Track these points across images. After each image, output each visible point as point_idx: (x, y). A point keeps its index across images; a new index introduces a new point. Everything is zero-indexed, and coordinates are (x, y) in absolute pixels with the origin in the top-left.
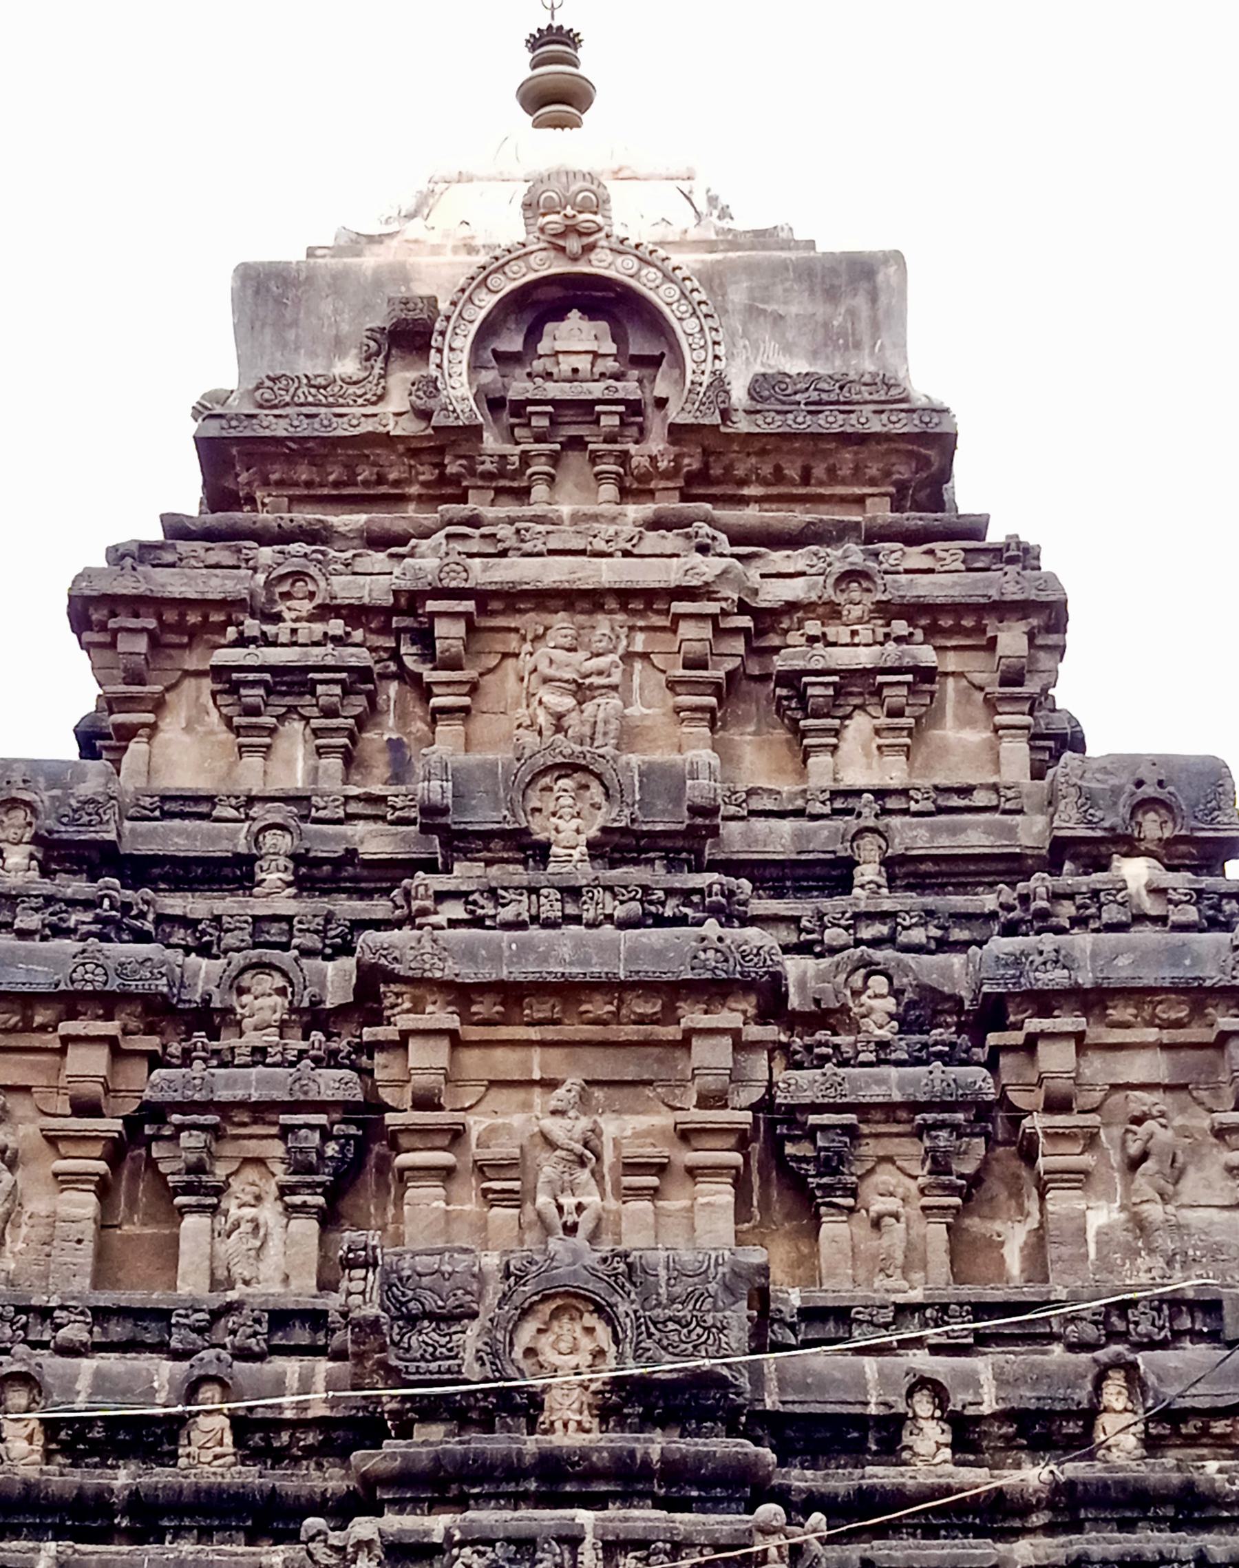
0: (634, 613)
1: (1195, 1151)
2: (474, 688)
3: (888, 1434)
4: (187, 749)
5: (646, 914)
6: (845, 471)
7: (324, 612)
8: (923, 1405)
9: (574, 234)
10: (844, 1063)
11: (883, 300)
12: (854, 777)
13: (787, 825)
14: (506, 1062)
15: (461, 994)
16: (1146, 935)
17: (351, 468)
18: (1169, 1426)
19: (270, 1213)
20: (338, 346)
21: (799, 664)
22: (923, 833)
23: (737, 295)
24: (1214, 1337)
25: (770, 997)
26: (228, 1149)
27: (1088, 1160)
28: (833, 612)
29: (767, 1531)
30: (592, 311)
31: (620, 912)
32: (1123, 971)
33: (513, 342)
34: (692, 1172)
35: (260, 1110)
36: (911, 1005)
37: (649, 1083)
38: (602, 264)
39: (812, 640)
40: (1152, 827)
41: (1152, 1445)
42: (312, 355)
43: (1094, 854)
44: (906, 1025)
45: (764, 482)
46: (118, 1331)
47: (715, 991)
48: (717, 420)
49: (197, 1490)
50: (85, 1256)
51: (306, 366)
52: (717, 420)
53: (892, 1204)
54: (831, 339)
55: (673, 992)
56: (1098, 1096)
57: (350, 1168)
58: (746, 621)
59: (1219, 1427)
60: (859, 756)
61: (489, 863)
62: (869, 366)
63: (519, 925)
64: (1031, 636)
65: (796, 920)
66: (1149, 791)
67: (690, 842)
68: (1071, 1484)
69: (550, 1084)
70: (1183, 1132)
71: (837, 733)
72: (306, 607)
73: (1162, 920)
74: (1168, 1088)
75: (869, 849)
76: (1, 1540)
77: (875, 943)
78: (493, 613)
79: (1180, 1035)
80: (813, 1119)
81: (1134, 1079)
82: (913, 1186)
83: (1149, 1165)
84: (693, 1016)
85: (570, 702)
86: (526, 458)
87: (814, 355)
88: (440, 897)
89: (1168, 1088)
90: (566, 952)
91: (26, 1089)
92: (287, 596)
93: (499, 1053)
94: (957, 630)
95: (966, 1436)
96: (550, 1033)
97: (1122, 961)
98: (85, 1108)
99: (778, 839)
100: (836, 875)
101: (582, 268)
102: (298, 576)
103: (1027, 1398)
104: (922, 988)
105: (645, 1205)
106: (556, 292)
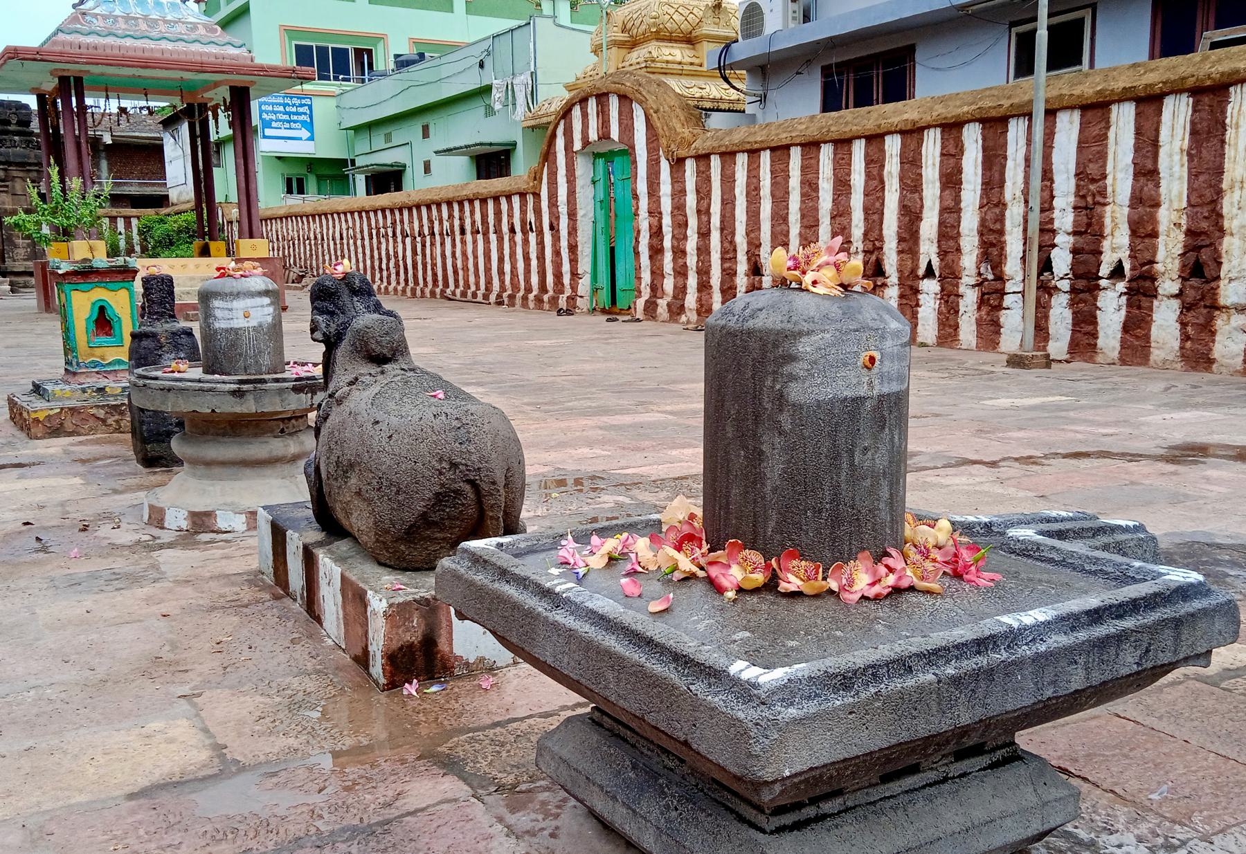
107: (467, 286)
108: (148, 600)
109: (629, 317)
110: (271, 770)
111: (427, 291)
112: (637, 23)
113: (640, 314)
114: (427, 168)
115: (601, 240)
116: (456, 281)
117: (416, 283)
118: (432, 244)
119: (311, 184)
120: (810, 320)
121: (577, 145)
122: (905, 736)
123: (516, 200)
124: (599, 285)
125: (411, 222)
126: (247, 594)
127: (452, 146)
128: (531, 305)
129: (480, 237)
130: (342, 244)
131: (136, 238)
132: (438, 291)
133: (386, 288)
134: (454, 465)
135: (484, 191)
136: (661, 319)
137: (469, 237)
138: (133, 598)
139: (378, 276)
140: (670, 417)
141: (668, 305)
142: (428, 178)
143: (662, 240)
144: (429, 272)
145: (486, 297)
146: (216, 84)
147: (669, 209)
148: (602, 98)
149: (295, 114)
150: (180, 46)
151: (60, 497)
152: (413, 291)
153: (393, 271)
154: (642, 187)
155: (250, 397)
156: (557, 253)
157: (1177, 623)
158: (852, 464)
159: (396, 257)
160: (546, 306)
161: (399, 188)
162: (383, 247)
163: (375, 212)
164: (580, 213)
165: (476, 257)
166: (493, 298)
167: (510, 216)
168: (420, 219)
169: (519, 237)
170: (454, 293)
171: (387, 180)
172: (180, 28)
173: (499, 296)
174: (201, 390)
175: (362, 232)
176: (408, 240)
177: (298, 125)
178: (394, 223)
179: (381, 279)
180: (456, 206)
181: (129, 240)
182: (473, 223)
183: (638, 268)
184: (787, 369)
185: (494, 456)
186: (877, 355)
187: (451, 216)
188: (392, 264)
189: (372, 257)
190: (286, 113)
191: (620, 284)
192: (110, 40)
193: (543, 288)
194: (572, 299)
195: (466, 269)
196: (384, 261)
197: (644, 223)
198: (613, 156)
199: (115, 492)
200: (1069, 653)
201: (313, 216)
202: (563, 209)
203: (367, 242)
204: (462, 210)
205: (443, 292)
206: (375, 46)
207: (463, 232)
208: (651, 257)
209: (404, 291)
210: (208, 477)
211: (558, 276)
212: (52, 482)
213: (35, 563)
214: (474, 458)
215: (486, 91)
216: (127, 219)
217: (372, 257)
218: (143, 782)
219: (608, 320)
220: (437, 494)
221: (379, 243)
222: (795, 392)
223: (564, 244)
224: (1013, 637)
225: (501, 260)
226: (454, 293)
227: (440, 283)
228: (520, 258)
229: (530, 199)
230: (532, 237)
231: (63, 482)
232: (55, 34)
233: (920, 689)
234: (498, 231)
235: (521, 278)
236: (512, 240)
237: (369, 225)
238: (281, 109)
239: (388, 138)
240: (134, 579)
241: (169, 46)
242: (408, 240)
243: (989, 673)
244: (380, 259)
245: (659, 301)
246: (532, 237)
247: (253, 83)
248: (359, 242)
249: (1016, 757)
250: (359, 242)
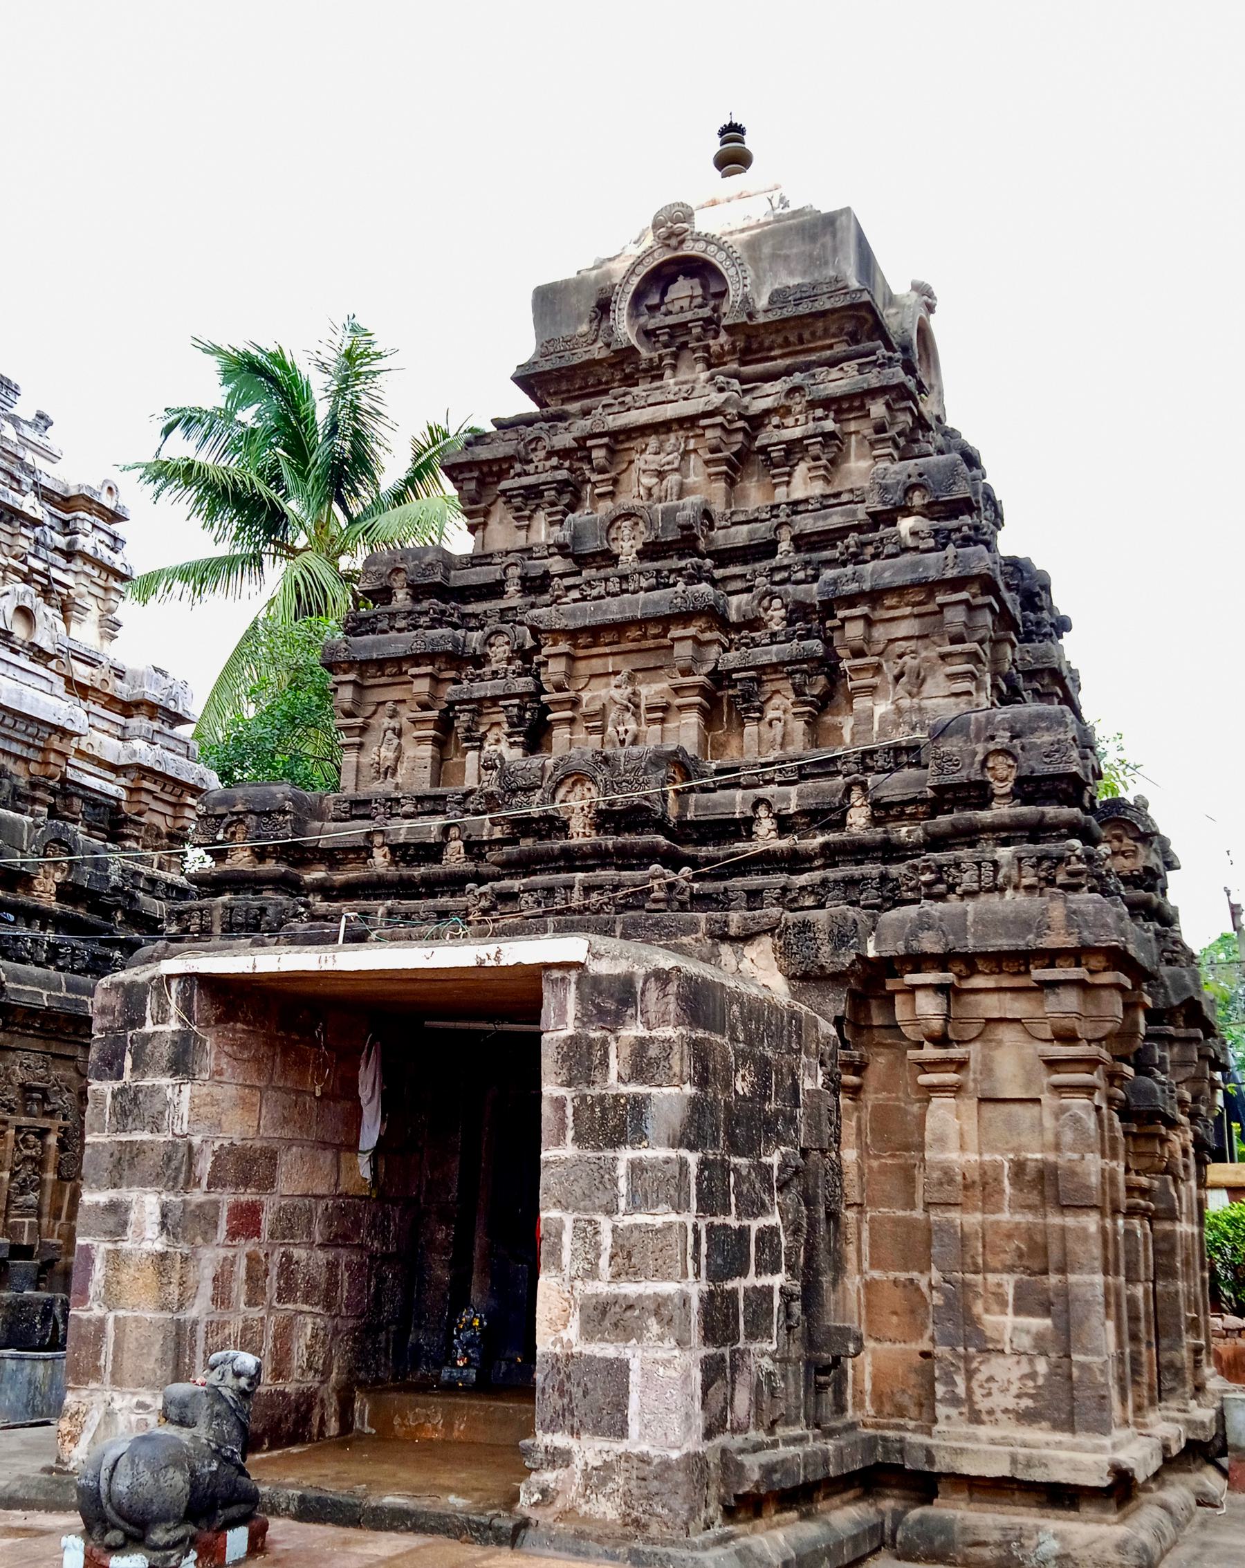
0: (687, 429)
1: (932, 669)
2: (615, 482)
3: (743, 828)
5: (658, 583)
6: (820, 333)
7: (550, 454)
8: (762, 811)
10: (757, 646)
11: (839, 235)
12: (798, 494)
13: (745, 528)
14: (597, 665)
15: (571, 635)
16: (907, 558)
17: (585, 379)
18: (882, 812)
19: (503, 747)
20: (579, 320)
21: (766, 442)
22: (811, 521)
23: (766, 250)
24: (918, 765)
25: (715, 616)
26: (485, 720)
27: (876, 680)
28: (787, 411)
29: (655, 877)
30: (690, 274)
31: (644, 584)
32: (888, 578)
33: (654, 299)
34: (681, 708)
35: (494, 700)
36: (792, 612)
37: (661, 667)
39: (776, 427)
40: (918, 499)
41: (875, 821)
42: (568, 326)
43: (888, 518)
44: (790, 621)
45: (781, 347)
46: (428, 806)
47: (684, 618)
48: (745, 319)
49: (445, 874)
50: (427, 774)
51: (566, 332)
52: (745, 319)
53: (778, 714)
55: (666, 621)
56: (882, 646)
58: (741, 424)
59: (909, 810)
61: (598, 568)
62: (832, 273)
63: (601, 597)
64: (888, 405)
65: (744, 576)
66: (913, 480)
67: (686, 544)
68: (624, 845)
69: (616, 673)
70: (926, 660)
71: (790, 474)
72: (542, 454)
73: (916, 549)
74: (919, 638)
75: (785, 536)
77: (783, 582)
78: (622, 442)
79: (923, 609)
80: (734, 676)
81: (900, 635)
82: (789, 702)
83: (904, 679)
84: (676, 632)
85: (655, 480)
86: (661, 358)
87: (804, 273)
88: (568, 588)
89: (919, 638)
90: (615, 608)
91: (404, 701)
92: (535, 450)
93: (594, 661)
94: (850, 410)
95: (784, 825)
96: (615, 648)
97: (887, 574)
98: (425, 707)
99: (740, 536)
100: (768, 549)
101: (680, 253)
102: (539, 439)
103: (811, 803)
104: (796, 602)
105: (658, 727)
106: (673, 268)
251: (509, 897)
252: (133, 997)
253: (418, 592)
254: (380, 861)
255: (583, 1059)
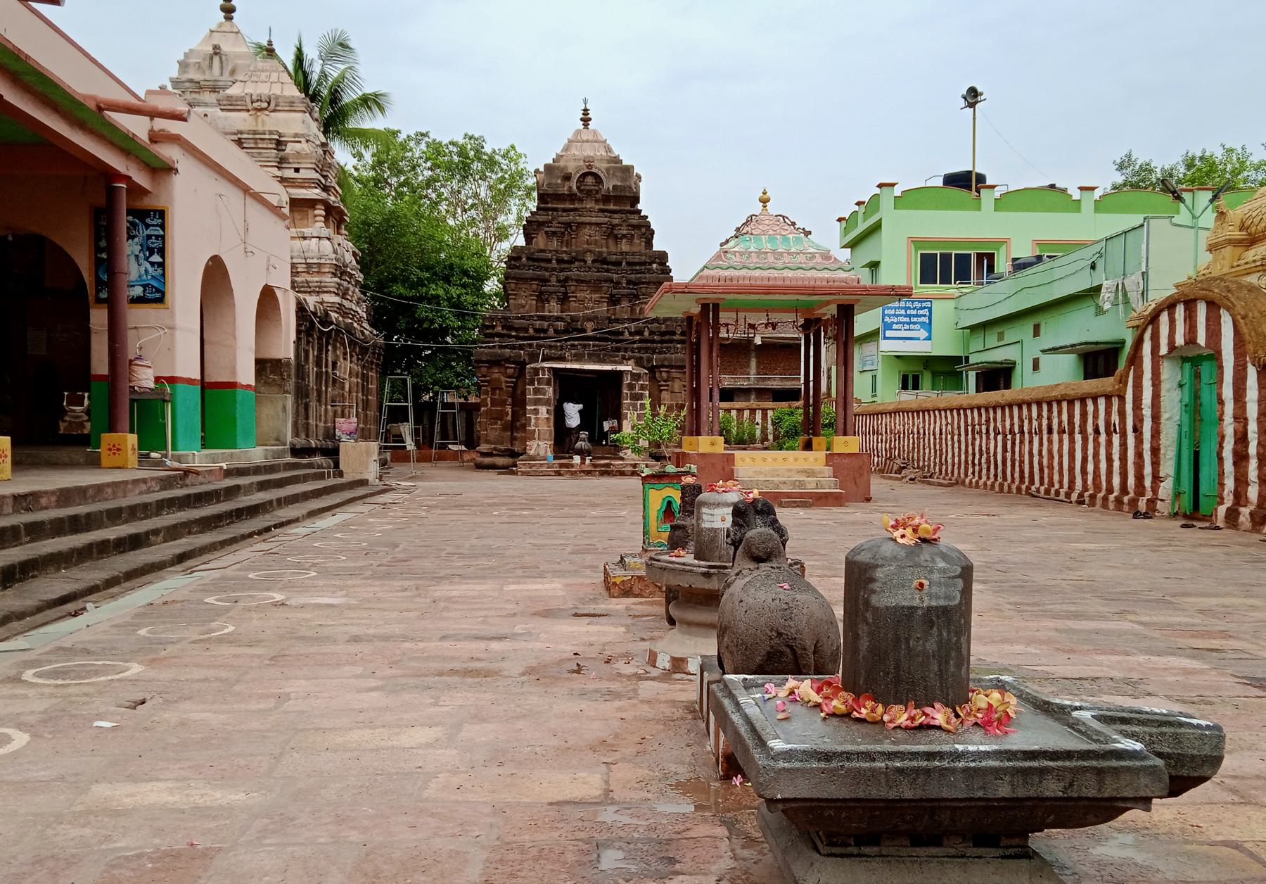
3: (622, 333)
4: (540, 241)
9: (589, 167)
15: (577, 281)
18: (651, 333)
25: (612, 281)
38: (594, 170)
43: (650, 264)
54: (623, 180)
57: (564, 299)
60: (624, 246)
76: (1, 726)
95: (631, 333)
100: (620, 264)
107: (1051, 484)
108: (619, 709)
109: (1207, 524)
110: (626, 806)
111: (1014, 487)
112: (1257, 220)
113: (1220, 522)
114: (1036, 366)
115: (1185, 442)
116: (1042, 478)
117: (1005, 479)
118: (1022, 442)
119: (926, 380)
120: (884, 558)
121: (1164, 350)
122: (861, 795)
123: (1102, 403)
124: (1181, 489)
125: (1003, 420)
126: (679, 713)
127: (1057, 345)
128: (1111, 506)
129: (1066, 437)
130: (941, 439)
131: (770, 428)
132: (1024, 487)
133: (977, 482)
134: (780, 634)
135: (1072, 392)
136: (1243, 528)
137: (1055, 437)
138: (609, 708)
139: (970, 470)
140: (1136, 626)
141: (1251, 514)
142: (1037, 375)
143: (1247, 447)
144: (1017, 469)
145: (1068, 495)
146: (828, 303)
147: (1256, 415)
148: (1190, 304)
149: (914, 316)
150: (799, 273)
151: (604, 639)
152: (1001, 485)
153: (984, 466)
154: (1228, 392)
155: (715, 578)
156: (1139, 455)
157: (1100, 772)
158: (908, 646)
159: (988, 453)
160: (1126, 508)
161: (1008, 386)
162: (977, 443)
163: (972, 410)
164: (1164, 416)
165: (1061, 456)
166: (1074, 496)
167: (1096, 417)
168: (1012, 418)
169: (1103, 438)
170: (1038, 490)
171: (997, 376)
172: (801, 258)
173: (1081, 495)
174: (684, 570)
175: (959, 428)
176: (1000, 438)
177: (918, 326)
178: (988, 421)
179: (973, 473)
180: (1045, 407)
181: (764, 430)
182: (1060, 423)
183: (1221, 474)
184: (870, 586)
185: (807, 630)
186: (926, 583)
187: (1040, 416)
188: (983, 460)
189: (967, 452)
190: (906, 316)
191: (1204, 489)
192: (744, 272)
193: (1124, 489)
194: (1152, 502)
195: (1051, 467)
196: (977, 456)
197: (1229, 429)
198: (1197, 360)
199: (643, 639)
200: (996, 772)
201: (918, 412)
202: (1147, 412)
203: (963, 438)
204: (1050, 411)
205: (1028, 488)
206: (998, 249)
207: (1050, 431)
208: (1235, 464)
209: (993, 486)
210: (690, 634)
211: (1140, 478)
212: (606, 628)
213: (568, 679)
214: (793, 631)
215: (1098, 289)
216: (765, 411)
217: (967, 452)
218: (560, 798)
219: (1183, 526)
220: (768, 653)
221: (974, 439)
222: (874, 600)
223: (1147, 446)
224: (958, 756)
225: (1085, 460)
226: (1038, 490)
227: (1027, 480)
228: (1103, 460)
229: (1115, 401)
230: (1116, 439)
231: (613, 629)
232: (702, 270)
233: (873, 770)
234: (1083, 432)
235: (1103, 478)
236: (1096, 441)
237: (966, 422)
238: (903, 312)
239: (1001, 336)
240: (617, 696)
241: (790, 274)
242: (1000, 438)
243: (928, 772)
244: (974, 454)
245: (1242, 509)
246: (1116, 439)
247: (858, 301)
248: (956, 438)
249: (1028, 854)
250: (956, 438)
251: (573, 346)
252: (536, 371)
253: (528, 259)
254: (531, 331)
255: (631, 387)
